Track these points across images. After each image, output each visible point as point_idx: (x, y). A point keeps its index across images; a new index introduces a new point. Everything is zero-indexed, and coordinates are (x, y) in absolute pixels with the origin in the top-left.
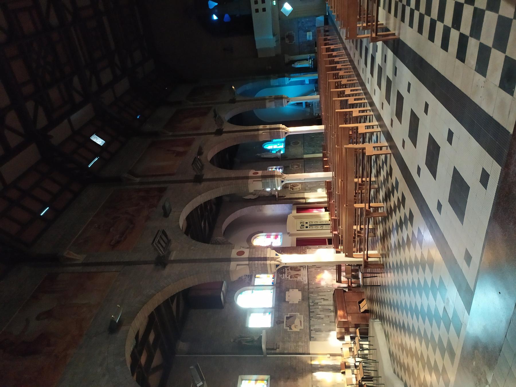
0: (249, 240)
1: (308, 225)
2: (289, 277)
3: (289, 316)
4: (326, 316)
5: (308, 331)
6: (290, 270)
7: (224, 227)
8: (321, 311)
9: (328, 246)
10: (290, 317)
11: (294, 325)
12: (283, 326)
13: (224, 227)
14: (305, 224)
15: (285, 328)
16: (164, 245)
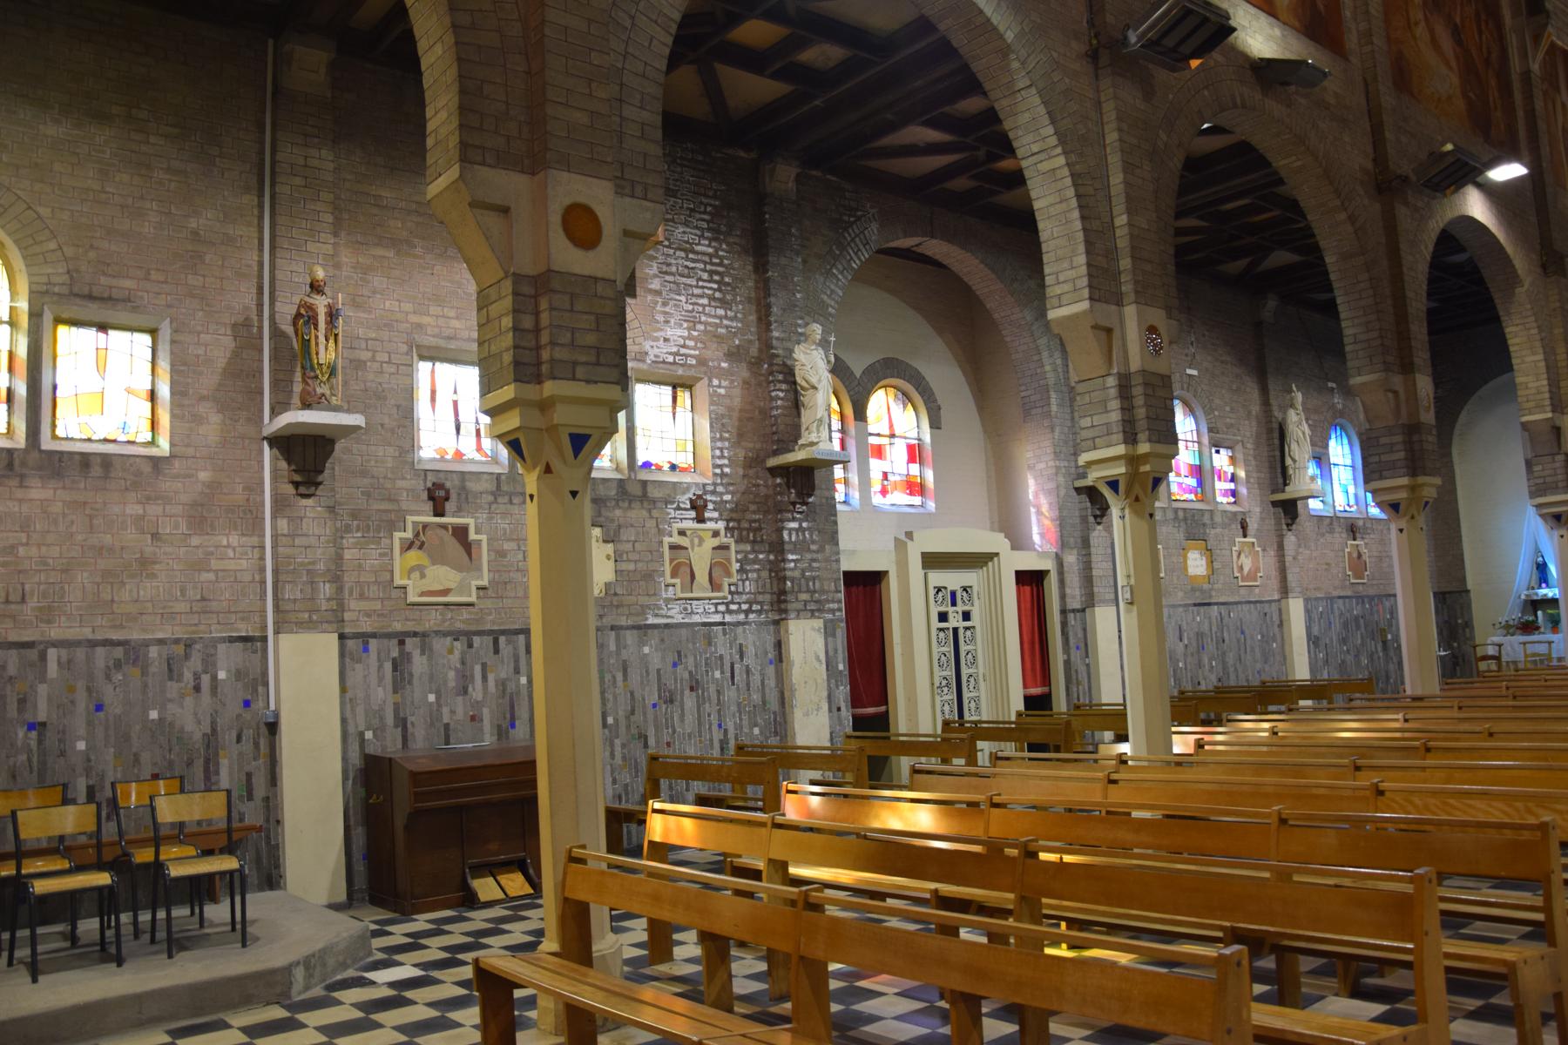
0: (889, 370)
1: (955, 621)
2: (676, 539)
3: (472, 536)
4: (477, 705)
5: (398, 627)
6: (716, 542)
7: (935, 248)
8: (502, 684)
9: (847, 715)
10: (467, 546)
11: (425, 561)
12: (418, 513)
13: (935, 248)
14: (960, 608)
15: (410, 519)
16: (1170, 42)
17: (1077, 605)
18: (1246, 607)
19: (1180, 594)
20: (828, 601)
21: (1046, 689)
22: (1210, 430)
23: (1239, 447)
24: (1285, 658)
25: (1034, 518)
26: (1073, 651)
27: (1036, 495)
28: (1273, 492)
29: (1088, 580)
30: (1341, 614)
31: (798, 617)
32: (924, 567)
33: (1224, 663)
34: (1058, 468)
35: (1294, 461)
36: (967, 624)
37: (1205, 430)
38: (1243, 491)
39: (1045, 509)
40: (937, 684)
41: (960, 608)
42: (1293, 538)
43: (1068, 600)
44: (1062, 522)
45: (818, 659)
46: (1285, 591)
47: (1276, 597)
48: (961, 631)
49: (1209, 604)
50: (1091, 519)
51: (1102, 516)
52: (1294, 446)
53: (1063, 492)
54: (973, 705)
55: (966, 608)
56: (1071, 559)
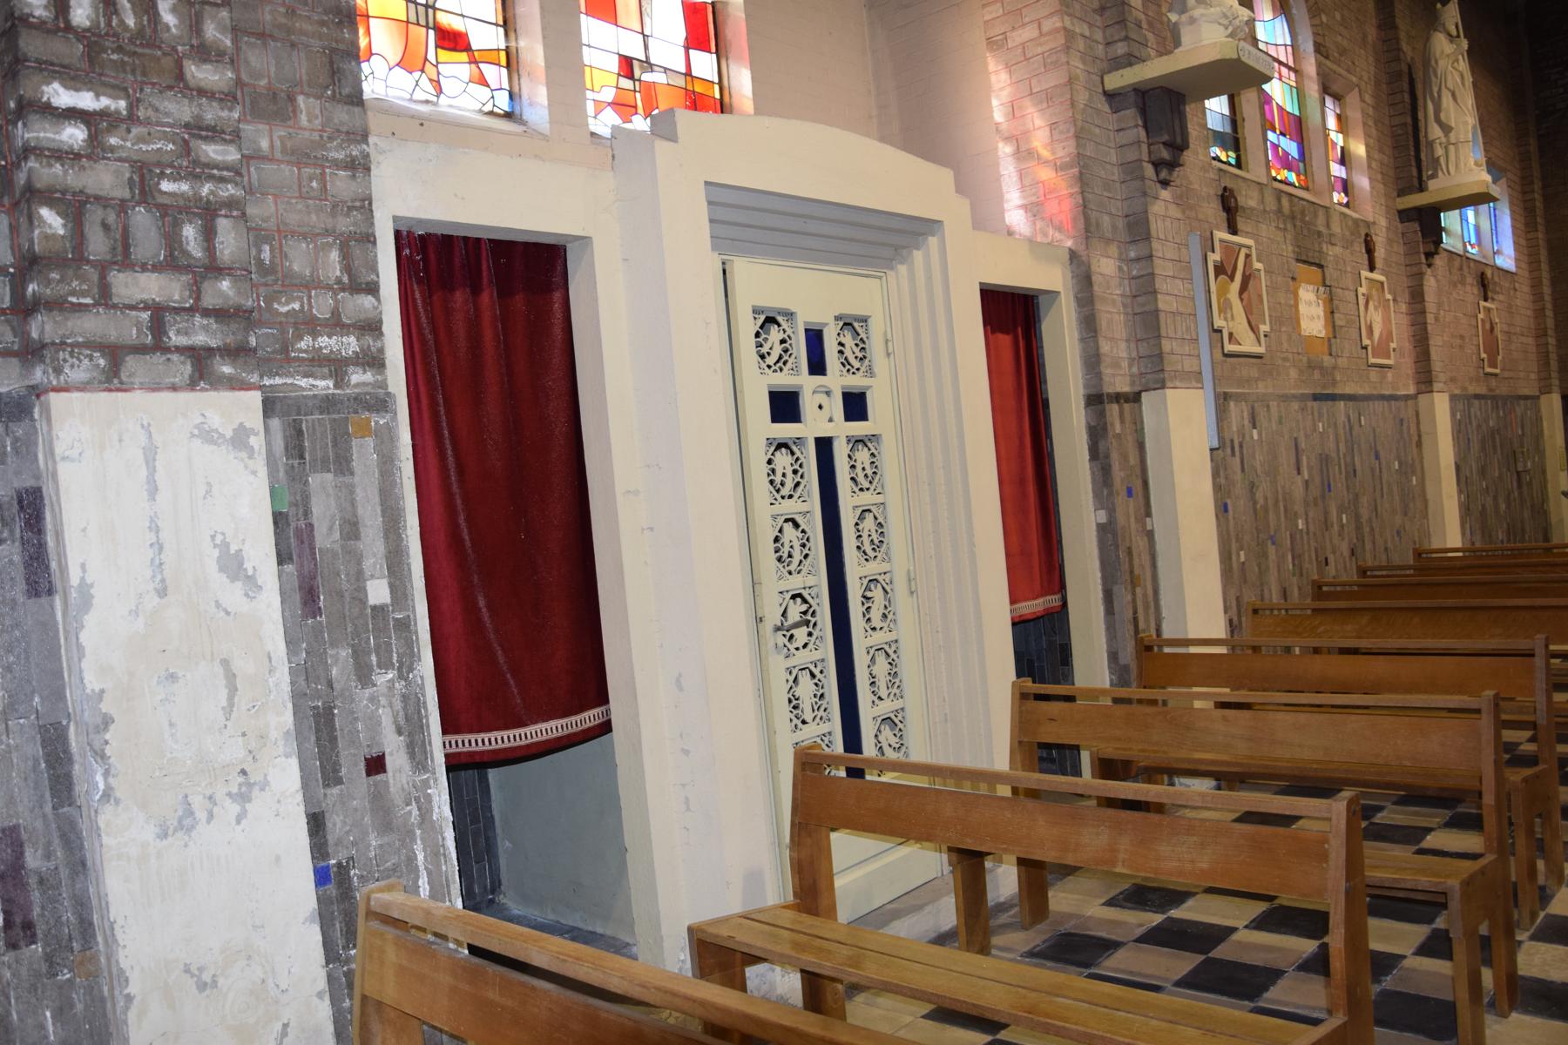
1: (821, 416)
14: (837, 379)
17: (1123, 386)
18: (1379, 406)
19: (1293, 373)
20: (311, 325)
21: (1053, 600)
22: (1319, 49)
23: (1353, 99)
24: (1415, 501)
25: (1008, 170)
26: (1120, 499)
27: (1013, 111)
28: (1402, 193)
29: (1147, 323)
30: (1479, 426)
31: (112, 378)
32: (718, 242)
33: (1357, 517)
34: (1070, 35)
35: (1447, 129)
36: (858, 428)
37: (1308, 47)
38: (1363, 182)
39: (1040, 140)
40: (773, 618)
41: (837, 379)
42: (1432, 280)
43: (1107, 371)
44: (1083, 172)
45: (233, 566)
46: (1425, 380)
47: (1412, 390)
48: (840, 451)
49: (1333, 398)
50: (1149, 170)
51: (1173, 165)
52: (1447, 100)
53: (1082, 97)
54: (881, 667)
55: (855, 382)
56: (1106, 266)
